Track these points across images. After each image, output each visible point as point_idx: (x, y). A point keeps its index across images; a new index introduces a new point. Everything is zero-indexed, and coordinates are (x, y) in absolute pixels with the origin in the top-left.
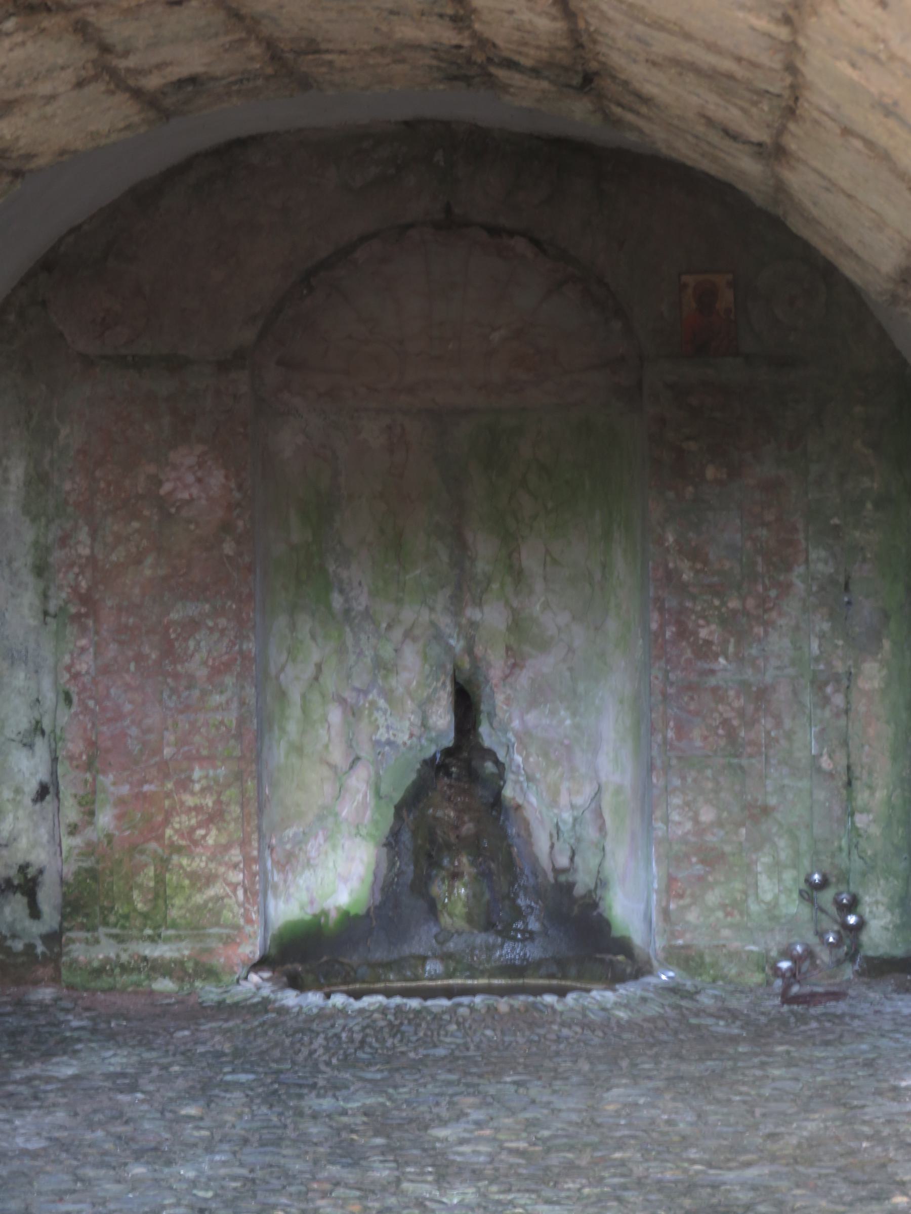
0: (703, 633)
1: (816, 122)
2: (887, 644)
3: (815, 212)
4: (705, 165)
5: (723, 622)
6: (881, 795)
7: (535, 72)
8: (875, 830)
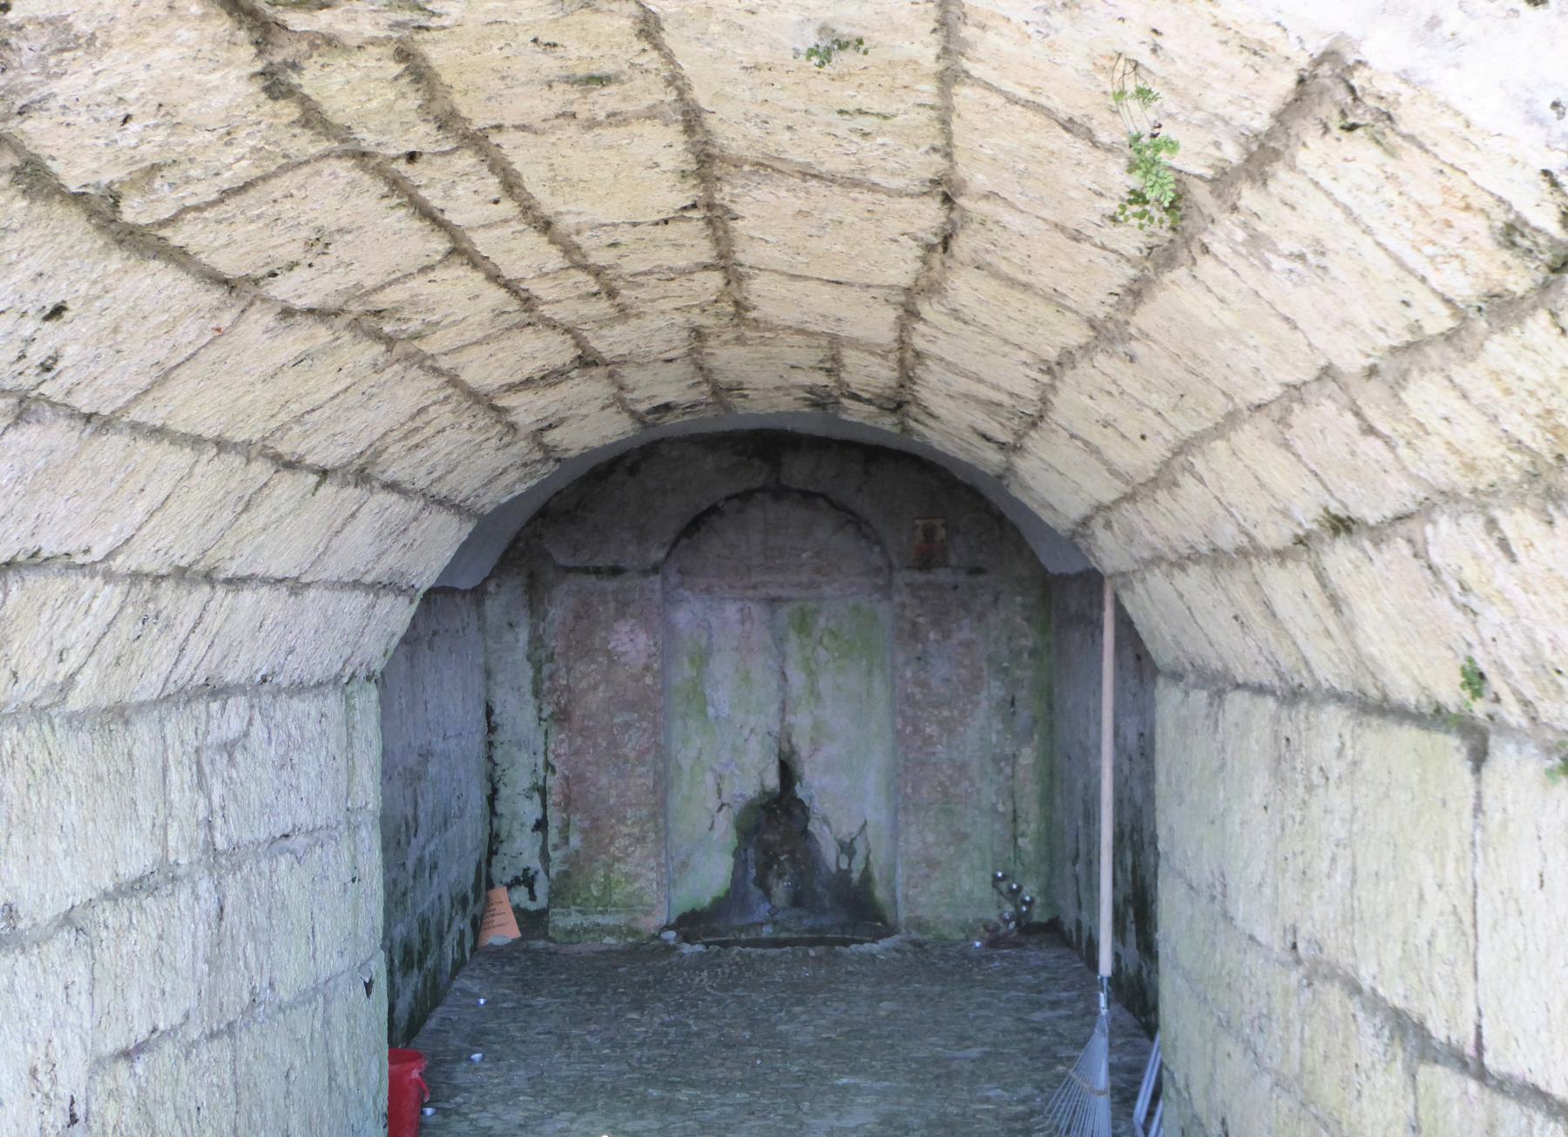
0: (928, 730)
1: (1053, 431)
2: (1036, 737)
3: (1032, 483)
4: (962, 456)
5: (940, 723)
6: (1033, 826)
7: (869, 402)
8: (1030, 848)
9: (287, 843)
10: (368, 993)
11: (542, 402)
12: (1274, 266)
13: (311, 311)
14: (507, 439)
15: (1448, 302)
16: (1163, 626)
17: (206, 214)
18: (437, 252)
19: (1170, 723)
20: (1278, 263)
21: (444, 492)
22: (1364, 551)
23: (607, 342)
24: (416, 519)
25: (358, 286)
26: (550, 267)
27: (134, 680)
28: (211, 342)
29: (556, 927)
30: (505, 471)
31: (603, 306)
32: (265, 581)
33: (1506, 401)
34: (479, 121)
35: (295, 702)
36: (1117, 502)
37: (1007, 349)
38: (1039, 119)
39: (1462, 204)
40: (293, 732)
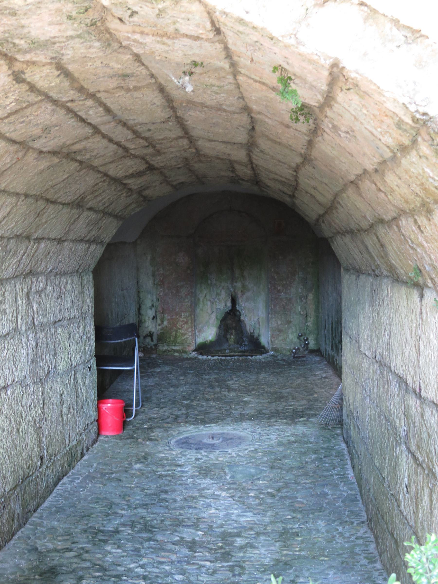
0: (279, 288)
2: (314, 290)
6: (312, 319)
7: (247, 181)
8: (311, 325)
9: (61, 323)
10: (90, 370)
11: (139, 182)
12: (342, 136)
13: (49, 152)
14: (129, 194)
15: (388, 147)
16: (343, 255)
17: (4, 121)
18: (89, 133)
19: (345, 286)
20: (343, 135)
21: (110, 211)
22: (386, 229)
23: (157, 161)
24: (100, 220)
25: (64, 143)
26: (129, 137)
27: (4, 271)
28: (15, 163)
29: (159, 350)
30: (131, 204)
31: (150, 150)
32: (49, 239)
33: (411, 180)
34: (92, 90)
35: (63, 279)
36: (324, 214)
37: (281, 164)
38: (264, 87)
39: (384, 114)
40: (62, 287)
